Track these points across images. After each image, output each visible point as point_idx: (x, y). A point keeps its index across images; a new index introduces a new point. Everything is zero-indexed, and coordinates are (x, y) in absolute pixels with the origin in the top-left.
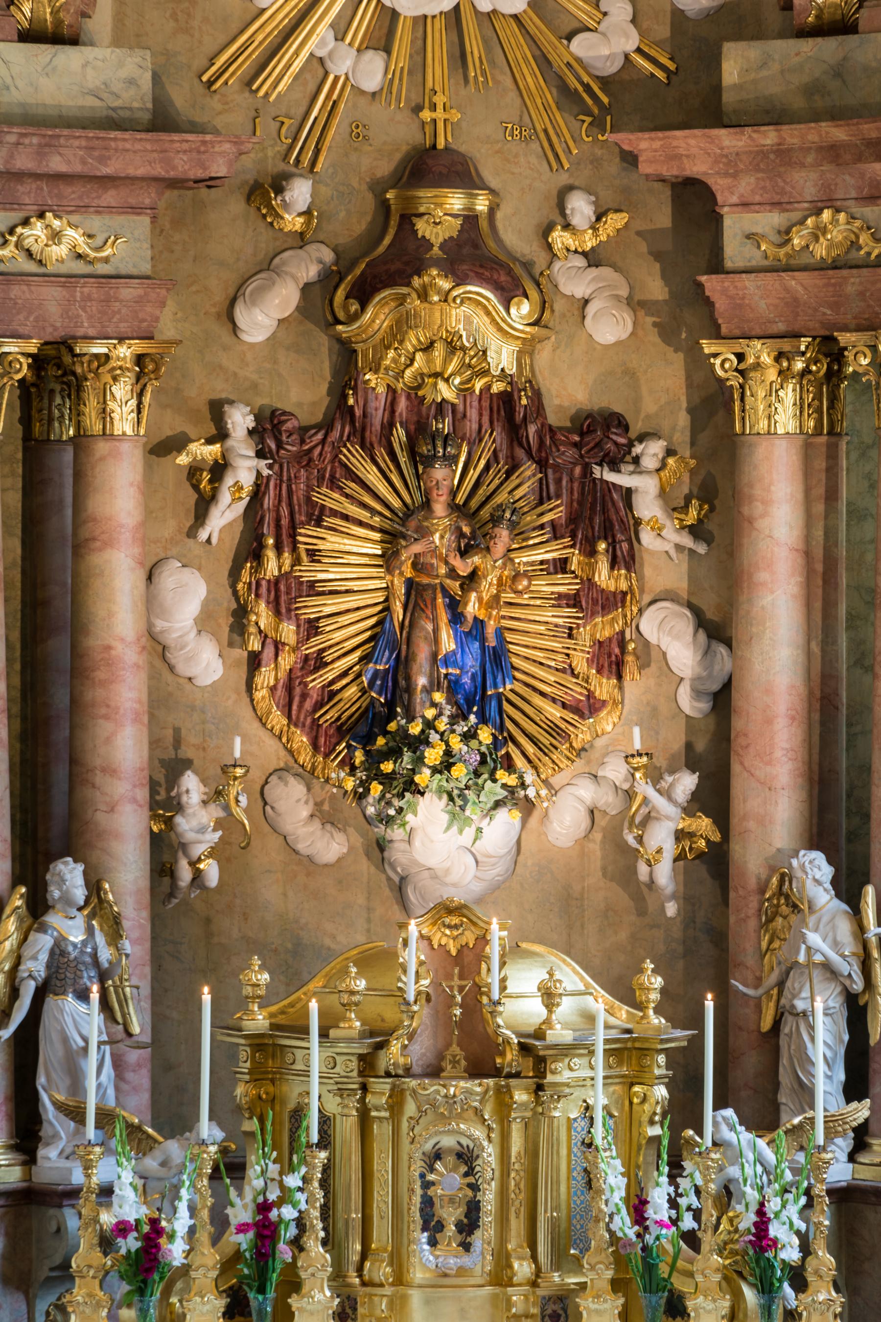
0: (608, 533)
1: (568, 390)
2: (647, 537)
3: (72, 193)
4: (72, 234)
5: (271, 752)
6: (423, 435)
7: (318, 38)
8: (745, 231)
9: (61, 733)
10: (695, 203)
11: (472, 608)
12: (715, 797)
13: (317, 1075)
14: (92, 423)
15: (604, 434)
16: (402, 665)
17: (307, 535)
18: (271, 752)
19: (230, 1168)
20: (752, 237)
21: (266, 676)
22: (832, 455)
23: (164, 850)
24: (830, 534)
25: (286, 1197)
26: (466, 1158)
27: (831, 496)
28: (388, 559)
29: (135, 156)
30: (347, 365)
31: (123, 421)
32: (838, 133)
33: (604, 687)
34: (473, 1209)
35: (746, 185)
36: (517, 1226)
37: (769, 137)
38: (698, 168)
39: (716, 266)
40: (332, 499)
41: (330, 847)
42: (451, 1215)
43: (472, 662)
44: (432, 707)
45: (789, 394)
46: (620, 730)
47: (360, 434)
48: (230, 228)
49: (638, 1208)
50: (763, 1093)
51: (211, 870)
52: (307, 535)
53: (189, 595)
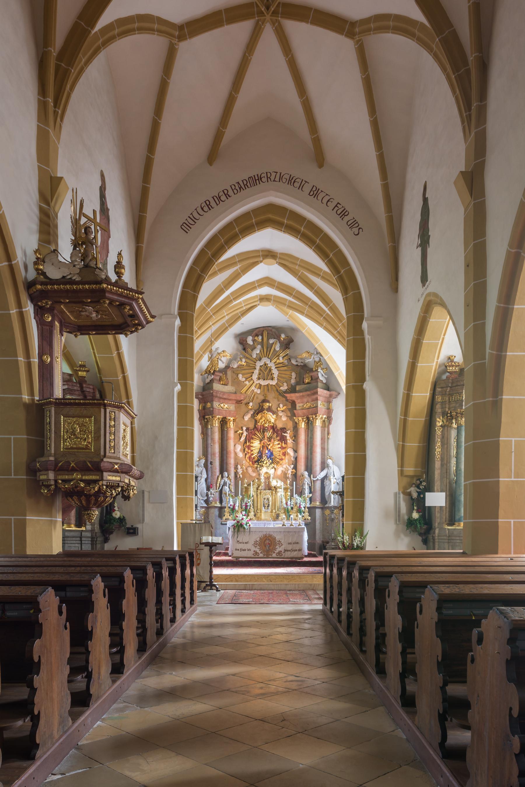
0: (284, 440)
1: (280, 425)
2: (288, 441)
3: (226, 401)
4: (226, 406)
5: (248, 464)
6: (264, 430)
7: (253, 388)
8: (299, 406)
9: (225, 461)
10: (293, 404)
11: (269, 447)
13: (252, 491)
14: (228, 426)
15: (284, 430)
16: (262, 454)
17: (252, 441)
18: (248, 464)
19: (242, 499)
20: (300, 407)
21: (247, 456)
22: (308, 431)
23: (236, 473)
24: (308, 440)
25: (249, 502)
26: (268, 499)
27: (308, 436)
28: (260, 443)
30: (256, 422)
31: (232, 427)
32: (309, 393)
33: (283, 457)
34: (269, 505)
35: (299, 401)
36: (273, 507)
37: (301, 394)
38: (294, 399)
39: (296, 409)
40: (253, 437)
41: (254, 475)
42: (266, 505)
43: (269, 454)
44: (265, 458)
45: (303, 423)
46: (286, 460)
47: (257, 430)
49: (287, 504)
50: (301, 493)
51: (241, 476)
52: (252, 441)
53: (239, 448)
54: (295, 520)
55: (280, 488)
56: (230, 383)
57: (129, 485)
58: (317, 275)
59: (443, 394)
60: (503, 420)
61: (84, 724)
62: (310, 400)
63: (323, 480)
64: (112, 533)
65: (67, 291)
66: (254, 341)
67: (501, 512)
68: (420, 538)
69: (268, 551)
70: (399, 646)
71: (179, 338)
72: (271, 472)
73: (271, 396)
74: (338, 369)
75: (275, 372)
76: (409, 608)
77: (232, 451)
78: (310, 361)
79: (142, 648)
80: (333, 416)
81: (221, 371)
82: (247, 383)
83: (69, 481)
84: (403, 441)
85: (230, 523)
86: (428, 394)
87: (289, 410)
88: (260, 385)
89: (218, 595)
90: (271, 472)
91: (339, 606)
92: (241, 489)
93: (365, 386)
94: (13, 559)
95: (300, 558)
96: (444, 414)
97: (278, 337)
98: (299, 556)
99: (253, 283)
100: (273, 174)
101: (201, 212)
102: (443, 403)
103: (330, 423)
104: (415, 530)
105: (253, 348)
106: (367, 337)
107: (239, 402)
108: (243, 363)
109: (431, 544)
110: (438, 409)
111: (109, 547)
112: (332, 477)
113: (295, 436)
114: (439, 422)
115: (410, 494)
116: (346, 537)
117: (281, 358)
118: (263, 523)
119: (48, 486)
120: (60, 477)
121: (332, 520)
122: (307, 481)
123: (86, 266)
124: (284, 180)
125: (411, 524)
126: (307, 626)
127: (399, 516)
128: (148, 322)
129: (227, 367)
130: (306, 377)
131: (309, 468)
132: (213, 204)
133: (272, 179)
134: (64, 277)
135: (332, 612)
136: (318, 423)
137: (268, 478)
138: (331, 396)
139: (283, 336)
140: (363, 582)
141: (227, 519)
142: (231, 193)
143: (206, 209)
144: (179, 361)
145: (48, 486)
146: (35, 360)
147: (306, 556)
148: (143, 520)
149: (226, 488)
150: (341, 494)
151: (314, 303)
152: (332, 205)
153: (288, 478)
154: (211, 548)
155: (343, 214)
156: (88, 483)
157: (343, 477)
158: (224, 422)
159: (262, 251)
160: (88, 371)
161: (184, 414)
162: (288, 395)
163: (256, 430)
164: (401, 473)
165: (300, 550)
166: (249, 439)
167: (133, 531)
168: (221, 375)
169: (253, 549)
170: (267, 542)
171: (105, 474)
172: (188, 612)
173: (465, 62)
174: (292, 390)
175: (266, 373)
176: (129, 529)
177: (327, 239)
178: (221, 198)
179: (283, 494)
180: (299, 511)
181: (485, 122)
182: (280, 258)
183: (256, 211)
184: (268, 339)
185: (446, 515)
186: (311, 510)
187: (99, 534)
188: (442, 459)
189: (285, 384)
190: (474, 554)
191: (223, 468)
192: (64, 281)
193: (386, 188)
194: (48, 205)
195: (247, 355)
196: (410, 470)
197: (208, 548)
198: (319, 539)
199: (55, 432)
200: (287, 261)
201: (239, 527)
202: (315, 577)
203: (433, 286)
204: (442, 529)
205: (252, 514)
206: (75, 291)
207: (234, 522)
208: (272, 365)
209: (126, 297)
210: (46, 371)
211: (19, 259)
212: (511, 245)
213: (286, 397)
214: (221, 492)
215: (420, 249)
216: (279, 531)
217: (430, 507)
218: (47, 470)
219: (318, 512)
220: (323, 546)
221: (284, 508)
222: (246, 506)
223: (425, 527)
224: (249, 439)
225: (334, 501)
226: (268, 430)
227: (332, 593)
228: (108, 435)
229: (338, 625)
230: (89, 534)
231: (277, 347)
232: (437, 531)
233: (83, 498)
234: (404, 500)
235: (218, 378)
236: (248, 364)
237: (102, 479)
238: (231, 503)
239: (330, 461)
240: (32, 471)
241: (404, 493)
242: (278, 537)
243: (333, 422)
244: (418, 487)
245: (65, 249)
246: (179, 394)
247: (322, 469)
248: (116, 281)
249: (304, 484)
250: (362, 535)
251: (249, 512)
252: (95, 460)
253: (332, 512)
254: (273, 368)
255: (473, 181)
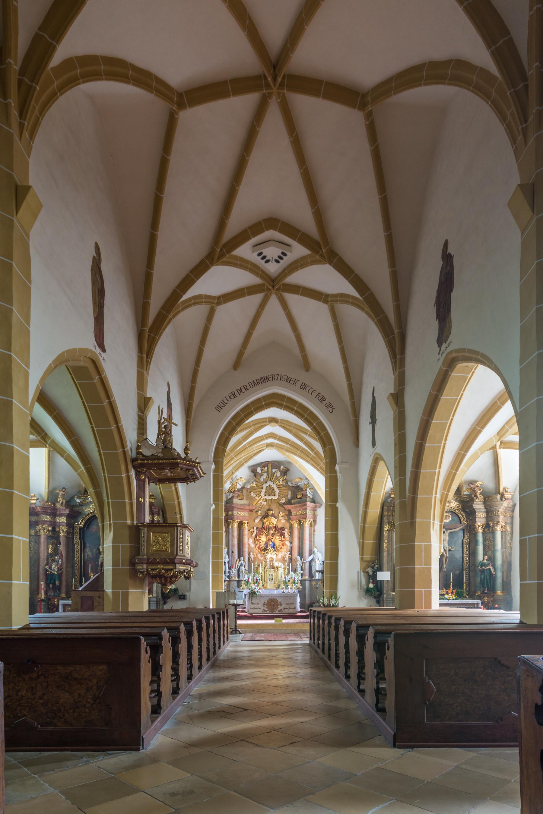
1: (280, 526)
6: (269, 529)
7: (261, 501)
10: (290, 512)
12: (291, 554)
13: (261, 569)
15: (283, 529)
19: (254, 575)
23: (249, 558)
26: (272, 575)
29: (247, 507)
30: (263, 524)
32: (300, 505)
37: (295, 505)
41: (262, 558)
44: (269, 547)
48: (254, 513)
49: (285, 578)
50: (295, 571)
53: (251, 541)
54: (291, 588)
55: (280, 567)
56: (245, 498)
57: (190, 571)
58: (306, 434)
59: (388, 511)
60: (416, 533)
61: (191, 686)
62: (301, 509)
63: (310, 562)
64: (169, 598)
65: (156, 464)
66: (262, 470)
67: (416, 585)
68: (375, 600)
69: (272, 609)
70: (344, 650)
71: (214, 476)
72: (274, 556)
73: (274, 507)
74: (321, 489)
75: (277, 491)
76: (361, 639)
77: (247, 543)
78: (301, 484)
79: (208, 660)
80: (318, 519)
81: (238, 490)
82: (257, 498)
83: (156, 569)
84: (363, 539)
85: (246, 591)
86: (378, 511)
87: (287, 515)
88: (266, 499)
89: (241, 636)
90: (274, 556)
91: (319, 639)
92: (252, 567)
93: (338, 505)
94: (120, 614)
95: (294, 614)
96: (389, 523)
97: (279, 468)
98: (294, 612)
99: (262, 436)
100: (276, 376)
101: (229, 399)
102: (388, 516)
103: (315, 524)
104: (371, 595)
105: (261, 475)
106: (339, 475)
107: (251, 511)
108: (254, 485)
109: (382, 603)
110: (385, 520)
111: (166, 607)
112: (317, 560)
113: (291, 533)
114: (386, 528)
115: (368, 572)
116: (326, 600)
117: (281, 482)
118: (270, 590)
119: (142, 573)
120: (150, 567)
121: (317, 588)
122: (299, 562)
123: (165, 447)
124: (283, 380)
125: (368, 591)
126: (299, 651)
127: (361, 586)
128: (201, 477)
129: (243, 488)
130: (298, 495)
131: (301, 554)
132: (237, 394)
133: (276, 378)
134: (153, 455)
135: (314, 643)
136: (307, 525)
137: (272, 561)
138: (316, 506)
139: (282, 467)
140: (337, 628)
141: (243, 589)
142: (248, 387)
143: (232, 397)
144: (214, 490)
145: (142, 573)
146: (135, 501)
147: (299, 612)
148: (190, 590)
149: (243, 568)
150: (322, 572)
151: (303, 449)
152: (315, 394)
153: (286, 561)
154: (236, 607)
155: (323, 400)
156: (167, 570)
157: (323, 562)
158: (241, 524)
159: (269, 418)
160: (155, 499)
161: (216, 521)
162: (286, 506)
163: (262, 529)
164: (362, 559)
165: (295, 608)
166: (258, 535)
167: (183, 597)
168: (239, 493)
169: (262, 608)
170: (272, 603)
171: (177, 565)
172: (226, 644)
173: (393, 333)
174: (289, 502)
175: (270, 491)
176: (180, 596)
177: (312, 414)
178: (242, 391)
179: (282, 571)
180: (294, 582)
181: (404, 366)
182: (280, 423)
183: (265, 398)
184: (272, 469)
185: (390, 586)
186: (302, 582)
187: (161, 599)
188: (388, 551)
189: (284, 499)
190: (400, 609)
191: (240, 554)
192: (153, 457)
193: (350, 386)
194: (143, 413)
195: (257, 480)
196: (367, 557)
197: (234, 607)
198: (308, 601)
199: (147, 542)
200: (285, 425)
201: (252, 594)
202: (304, 625)
203: (379, 449)
204: (388, 594)
205: (261, 585)
206: (160, 464)
207: (249, 591)
208: (274, 486)
209: (191, 466)
210: (141, 506)
211: (129, 446)
212: (417, 438)
213: (284, 508)
214: (239, 571)
215: (371, 425)
216: (280, 596)
217: (381, 581)
218: (143, 563)
219: (307, 583)
220: (311, 605)
221: (284, 581)
222: (257, 580)
223: (378, 593)
224: (258, 535)
225: (318, 576)
226: (272, 529)
227: (314, 632)
228: (179, 543)
229: (318, 649)
230: (155, 599)
231: (278, 474)
232: (385, 596)
233: (163, 579)
234: (364, 576)
235: (237, 495)
236: (257, 486)
237: (175, 568)
238: (246, 578)
239: (315, 550)
240: (133, 564)
241: (363, 572)
242: (279, 600)
243: (317, 524)
244: (373, 568)
245: (152, 436)
246: (214, 510)
247: (310, 555)
248: (185, 458)
249: (297, 565)
250: (336, 598)
251: (259, 583)
252: (171, 557)
253: (317, 583)
254: (275, 488)
255: (398, 398)
